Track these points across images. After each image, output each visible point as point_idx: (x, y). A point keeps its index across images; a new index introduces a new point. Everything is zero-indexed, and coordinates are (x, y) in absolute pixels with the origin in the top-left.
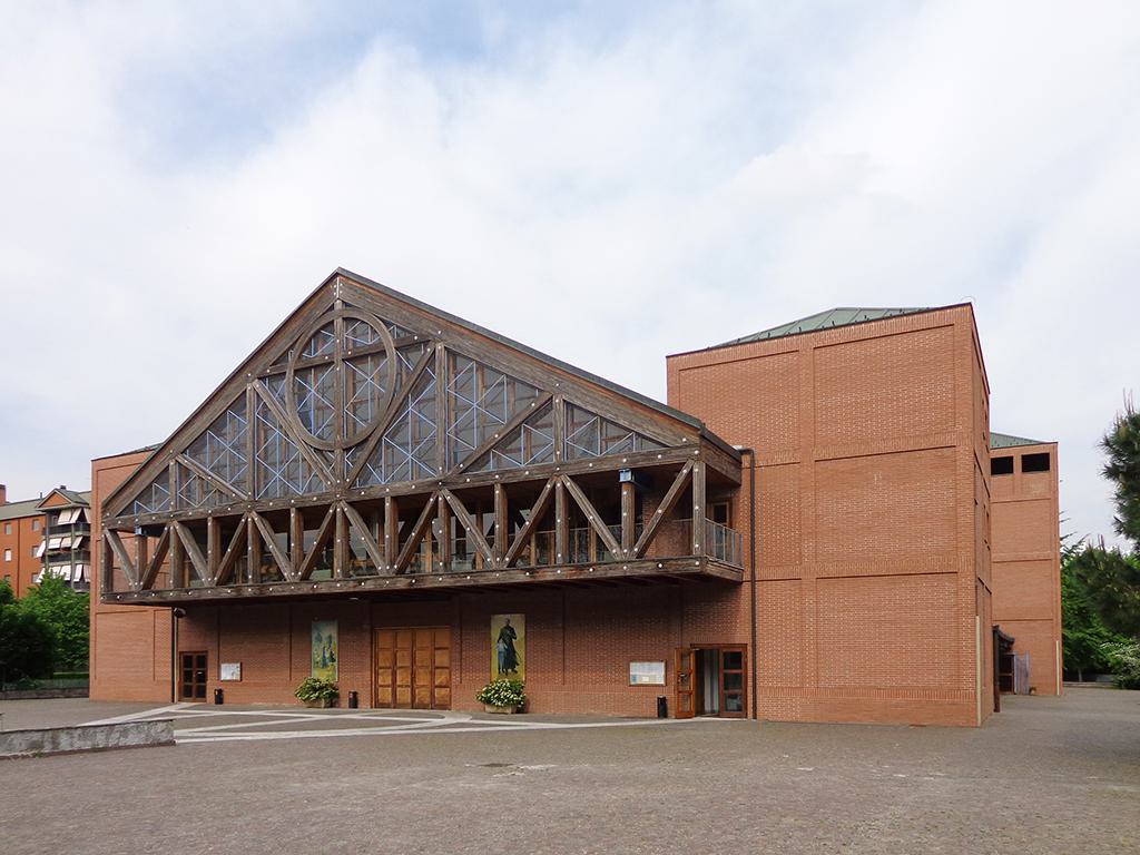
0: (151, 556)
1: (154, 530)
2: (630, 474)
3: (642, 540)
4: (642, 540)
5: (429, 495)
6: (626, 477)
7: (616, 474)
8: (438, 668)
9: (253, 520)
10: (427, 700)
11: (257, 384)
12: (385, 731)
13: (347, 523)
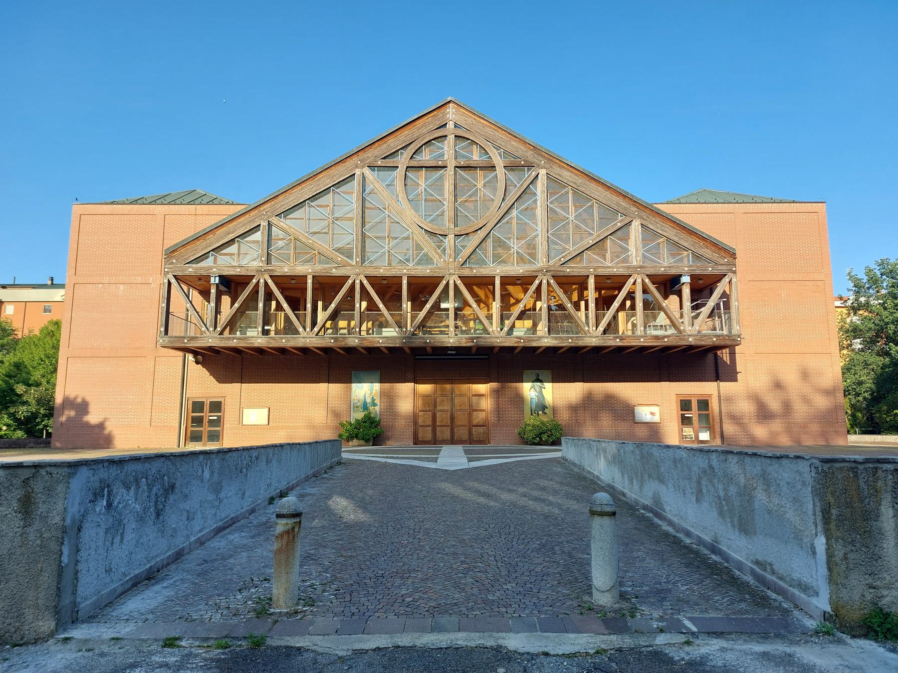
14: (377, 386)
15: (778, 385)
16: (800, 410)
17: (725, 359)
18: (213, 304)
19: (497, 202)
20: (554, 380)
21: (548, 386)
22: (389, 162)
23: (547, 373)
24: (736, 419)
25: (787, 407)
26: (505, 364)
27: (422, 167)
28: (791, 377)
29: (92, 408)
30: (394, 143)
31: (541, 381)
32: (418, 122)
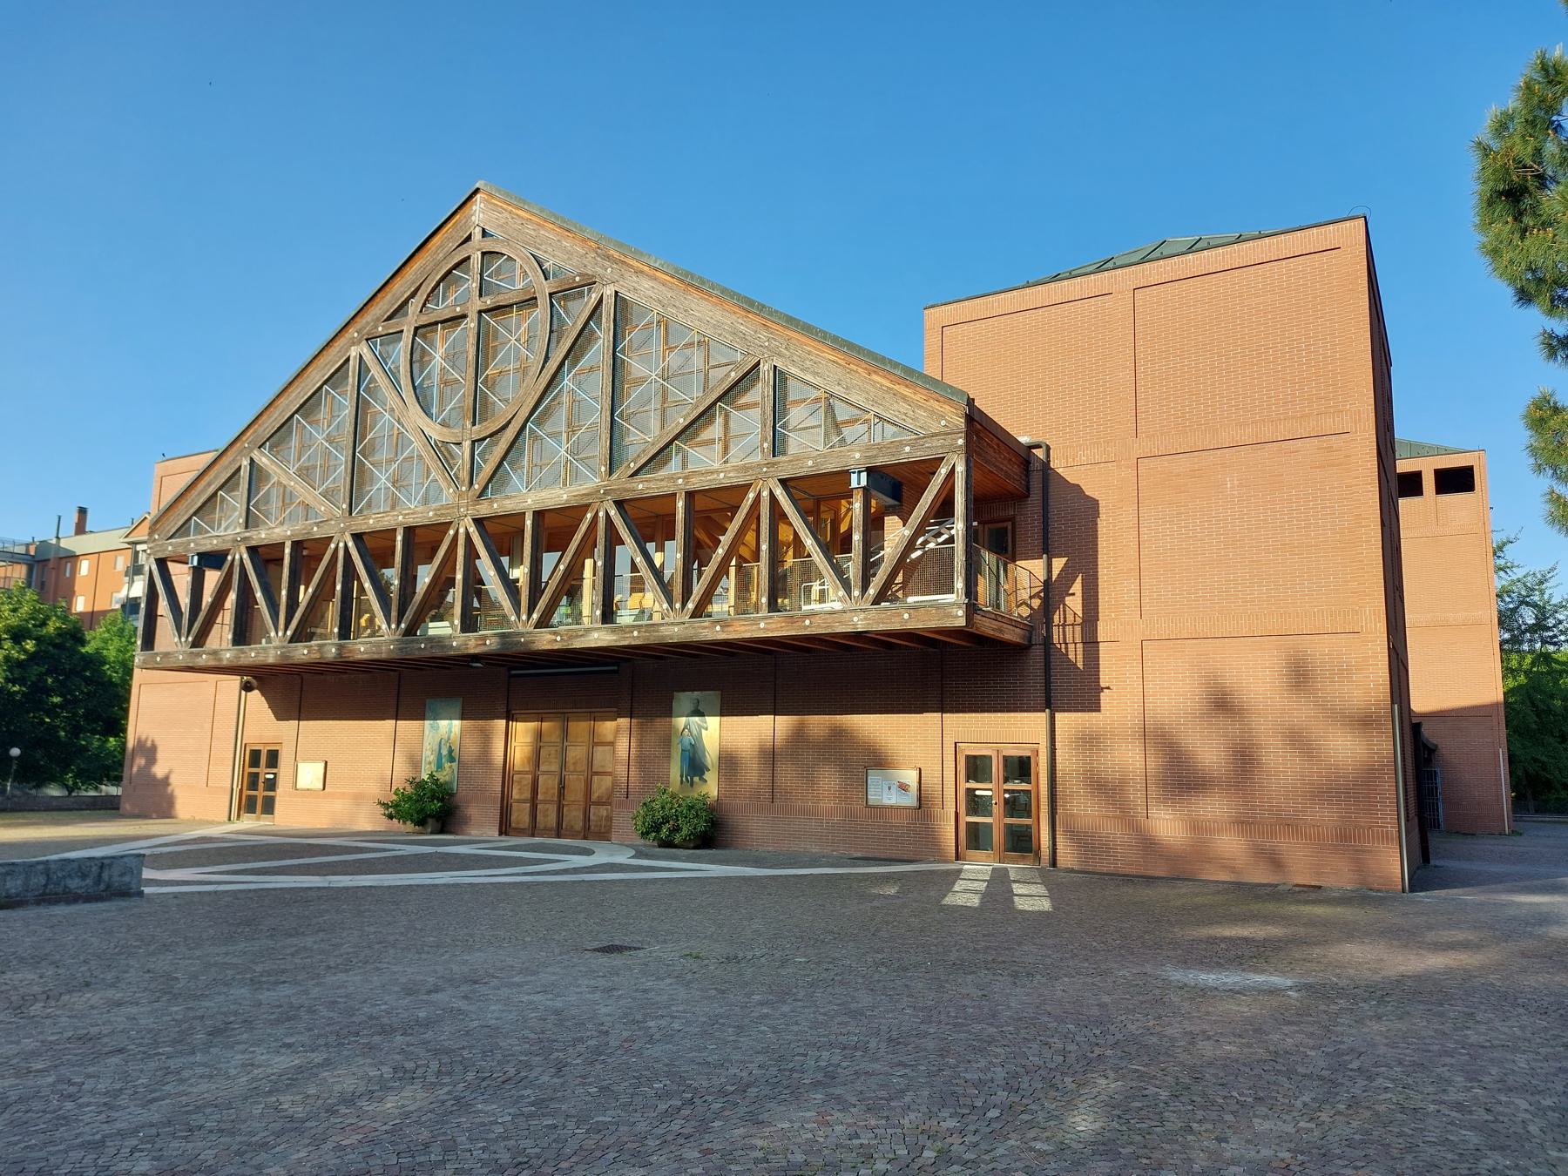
0: (207, 598)
1: (212, 559)
2: (864, 475)
3: (409, 614)
4: (409, 614)
5: (586, 507)
6: (858, 481)
7: (845, 474)
8: (597, 773)
9: (346, 546)
10: (579, 825)
11: (364, 349)
12: (503, 876)
13: (471, 554)
14: (457, 724)
15: (1222, 704)
16: (1281, 768)
17: (1072, 656)
18: (907, 532)
19: (535, 369)
20: (724, 713)
21: (713, 722)
22: (393, 326)
23: (713, 696)
24: (1105, 788)
25: (1245, 760)
26: (642, 680)
27: (436, 323)
28: (1257, 678)
29: (161, 755)
30: (400, 289)
31: (702, 715)
32: (429, 245)
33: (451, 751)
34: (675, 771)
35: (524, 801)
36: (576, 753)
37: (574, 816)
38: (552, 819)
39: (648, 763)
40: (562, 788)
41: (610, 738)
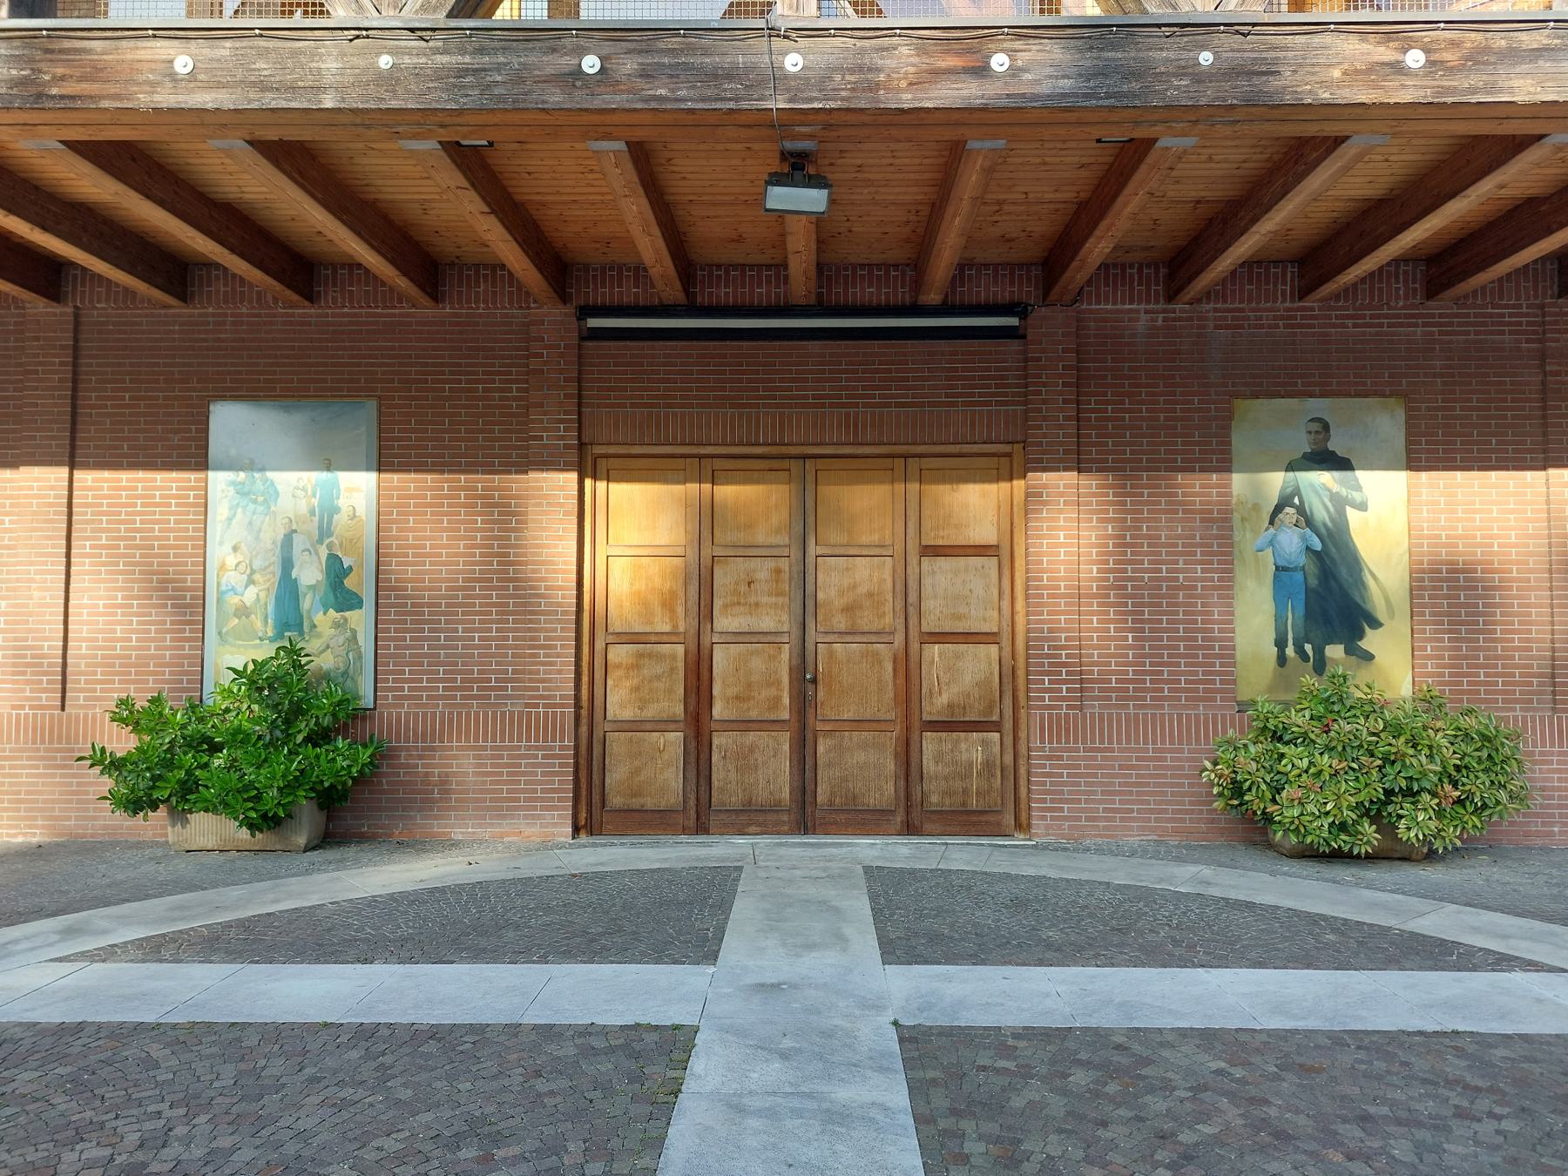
23: (362, 420)
31: (1341, 464)
33: (337, 573)
34: (1254, 620)
35: (661, 725)
36: (852, 577)
37: (859, 764)
38: (774, 772)
39: (1140, 594)
40: (805, 680)
41: (985, 533)
